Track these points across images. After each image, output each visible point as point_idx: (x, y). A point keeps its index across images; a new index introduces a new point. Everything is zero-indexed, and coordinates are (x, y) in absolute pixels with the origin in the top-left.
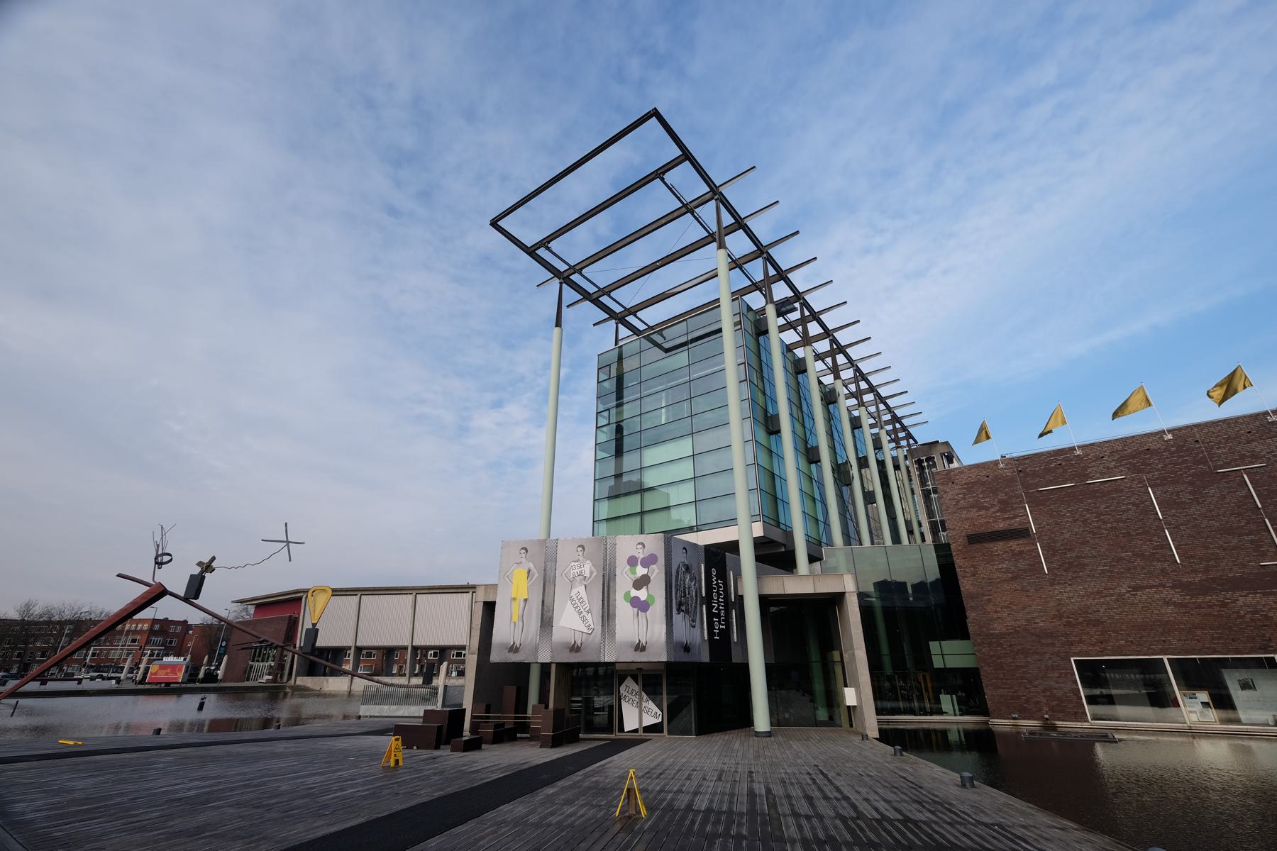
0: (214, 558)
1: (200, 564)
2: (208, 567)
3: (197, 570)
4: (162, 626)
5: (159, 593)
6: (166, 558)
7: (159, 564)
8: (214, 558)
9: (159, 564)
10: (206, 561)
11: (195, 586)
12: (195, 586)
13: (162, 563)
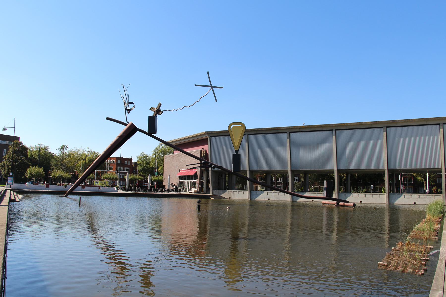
0: (160, 105)
1: (152, 109)
2: (158, 112)
3: (152, 114)
4: (121, 161)
5: (131, 130)
6: (131, 106)
7: (128, 110)
8: (160, 105)
9: (128, 110)
10: (155, 106)
11: (152, 122)
12: (152, 122)
13: (130, 110)
